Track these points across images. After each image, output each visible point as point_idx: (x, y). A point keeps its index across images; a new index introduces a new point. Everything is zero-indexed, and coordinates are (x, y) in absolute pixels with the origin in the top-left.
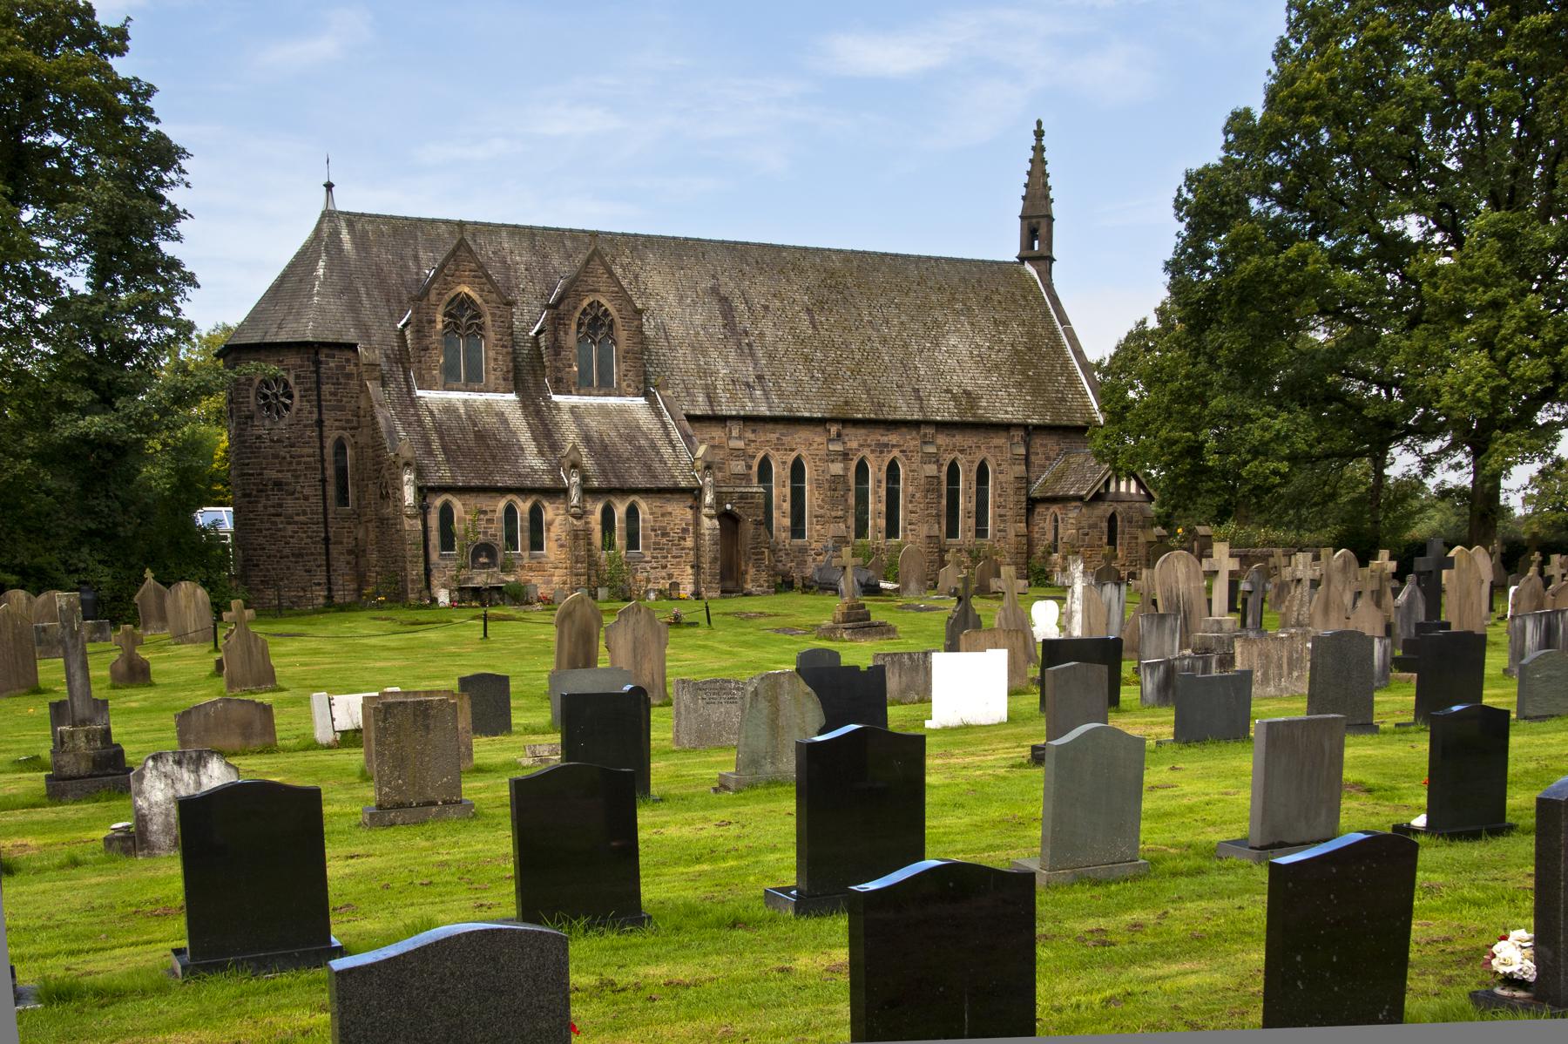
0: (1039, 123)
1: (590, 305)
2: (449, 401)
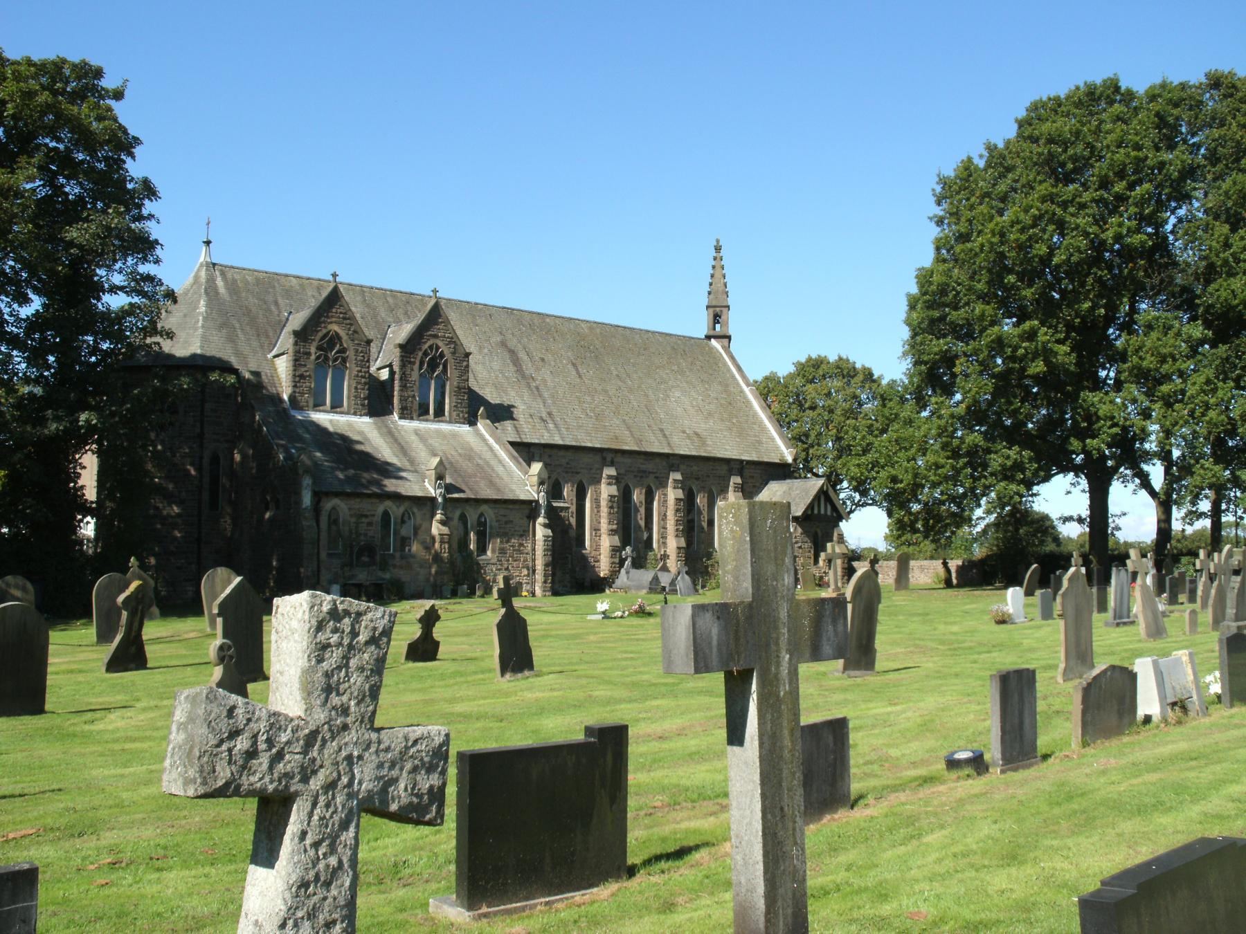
0: (718, 241)
1: (431, 347)
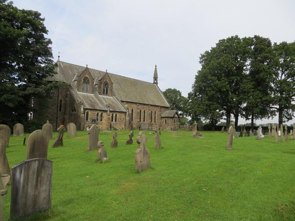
2: (83, 94)
